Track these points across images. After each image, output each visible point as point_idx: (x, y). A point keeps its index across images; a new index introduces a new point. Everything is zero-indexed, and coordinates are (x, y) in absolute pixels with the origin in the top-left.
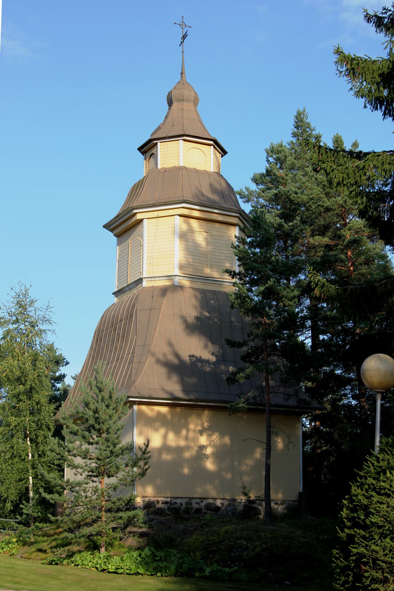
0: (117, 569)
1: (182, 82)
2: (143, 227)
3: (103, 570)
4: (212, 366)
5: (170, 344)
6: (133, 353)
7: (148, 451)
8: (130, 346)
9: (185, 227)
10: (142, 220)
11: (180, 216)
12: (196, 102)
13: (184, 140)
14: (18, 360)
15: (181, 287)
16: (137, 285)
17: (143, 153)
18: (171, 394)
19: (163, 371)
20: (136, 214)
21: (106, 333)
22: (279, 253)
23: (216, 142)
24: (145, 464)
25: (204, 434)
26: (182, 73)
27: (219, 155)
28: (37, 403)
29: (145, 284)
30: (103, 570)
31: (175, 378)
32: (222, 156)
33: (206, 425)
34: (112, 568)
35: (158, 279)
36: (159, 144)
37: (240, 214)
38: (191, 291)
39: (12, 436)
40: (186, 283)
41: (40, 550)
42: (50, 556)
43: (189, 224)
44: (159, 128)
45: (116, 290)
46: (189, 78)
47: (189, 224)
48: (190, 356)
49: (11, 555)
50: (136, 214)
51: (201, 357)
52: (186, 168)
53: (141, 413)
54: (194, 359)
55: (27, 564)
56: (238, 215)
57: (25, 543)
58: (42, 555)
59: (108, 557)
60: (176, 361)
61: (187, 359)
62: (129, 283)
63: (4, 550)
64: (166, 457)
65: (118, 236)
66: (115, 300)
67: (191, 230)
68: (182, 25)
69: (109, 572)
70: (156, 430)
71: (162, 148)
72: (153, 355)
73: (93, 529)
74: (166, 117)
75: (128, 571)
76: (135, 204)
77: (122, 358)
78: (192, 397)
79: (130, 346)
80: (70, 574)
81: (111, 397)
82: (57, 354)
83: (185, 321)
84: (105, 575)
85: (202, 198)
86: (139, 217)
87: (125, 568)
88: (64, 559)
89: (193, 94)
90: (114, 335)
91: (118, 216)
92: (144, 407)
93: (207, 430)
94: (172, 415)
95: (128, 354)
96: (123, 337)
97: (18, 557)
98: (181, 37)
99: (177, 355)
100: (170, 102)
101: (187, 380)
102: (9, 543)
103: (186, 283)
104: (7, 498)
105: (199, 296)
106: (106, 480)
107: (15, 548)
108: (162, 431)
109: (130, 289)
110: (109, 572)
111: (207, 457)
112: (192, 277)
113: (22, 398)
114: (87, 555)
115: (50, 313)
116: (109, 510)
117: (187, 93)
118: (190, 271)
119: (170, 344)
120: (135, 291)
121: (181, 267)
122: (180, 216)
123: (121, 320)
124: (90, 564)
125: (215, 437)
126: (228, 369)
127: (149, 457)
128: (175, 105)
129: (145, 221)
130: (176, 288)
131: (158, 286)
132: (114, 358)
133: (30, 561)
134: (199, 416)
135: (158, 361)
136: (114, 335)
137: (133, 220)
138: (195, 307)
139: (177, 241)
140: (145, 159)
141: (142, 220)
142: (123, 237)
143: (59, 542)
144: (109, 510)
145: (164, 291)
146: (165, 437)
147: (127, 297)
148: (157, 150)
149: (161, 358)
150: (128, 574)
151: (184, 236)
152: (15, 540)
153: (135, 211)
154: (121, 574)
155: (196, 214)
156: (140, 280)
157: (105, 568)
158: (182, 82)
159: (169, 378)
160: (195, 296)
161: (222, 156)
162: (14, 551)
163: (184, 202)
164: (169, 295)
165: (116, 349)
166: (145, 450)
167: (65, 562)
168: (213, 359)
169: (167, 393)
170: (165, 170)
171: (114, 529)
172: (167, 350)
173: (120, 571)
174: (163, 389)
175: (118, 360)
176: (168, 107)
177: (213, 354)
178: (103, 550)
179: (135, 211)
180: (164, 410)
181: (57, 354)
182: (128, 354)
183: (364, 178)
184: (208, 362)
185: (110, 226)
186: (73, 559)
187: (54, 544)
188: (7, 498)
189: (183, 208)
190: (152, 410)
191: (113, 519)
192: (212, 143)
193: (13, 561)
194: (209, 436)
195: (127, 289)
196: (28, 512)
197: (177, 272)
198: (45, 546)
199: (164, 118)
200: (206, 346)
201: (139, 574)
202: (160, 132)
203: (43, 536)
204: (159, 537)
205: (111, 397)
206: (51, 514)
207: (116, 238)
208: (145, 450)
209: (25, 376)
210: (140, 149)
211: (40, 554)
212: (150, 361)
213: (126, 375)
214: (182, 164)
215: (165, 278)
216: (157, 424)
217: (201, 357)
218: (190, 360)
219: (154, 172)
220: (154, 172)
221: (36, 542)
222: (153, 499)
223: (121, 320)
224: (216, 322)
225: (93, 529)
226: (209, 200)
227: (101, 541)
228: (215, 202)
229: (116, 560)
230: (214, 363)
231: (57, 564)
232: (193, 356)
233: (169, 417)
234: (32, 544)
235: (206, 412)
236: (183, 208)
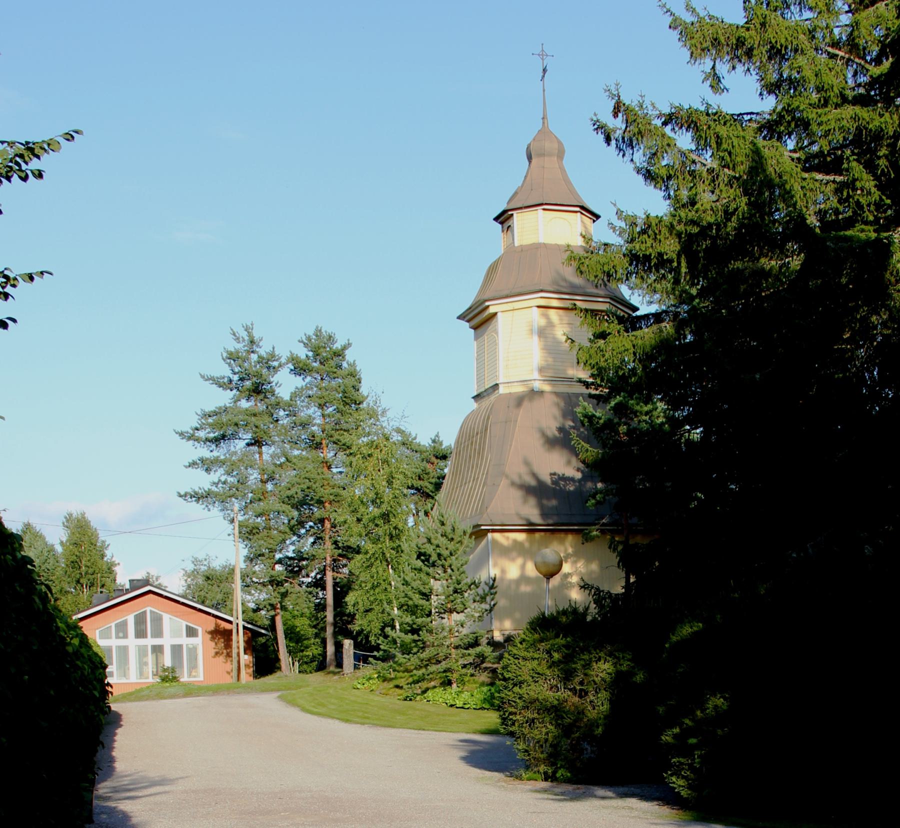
0: (465, 704)
1: (544, 132)
2: (497, 321)
3: (452, 706)
4: (577, 484)
5: (527, 463)
6: (487, 473)
7: (495, 585)
8: (485, 468)
9: (543, 322)
10: (495, 314)
11: (539, 307)
12: (561, 154)
13: (544, 209)
14: (372, 479)
15: (541, 393)
16: (494, 391)
17: (502, 223)
18: (528, 520)
19: (518, 494)
20: (488, 306)
21: (464, 447)
22: (347, 551)
23: (583, 208)
24: (492, 599)
25: (569, 560)
26: (543, 118)
27: (588, 221)
28: (395, 528)
29: (502, 390)
30: (452, 706)
31: (532, 501)
32: (594, 221)
33: (570, 550)
34: (459, 703)
35: (516, 384)
36: (515, 215)
37: (611, 298)
38: (554, 399)
39: (372, 565)
40: (547, 388)
41: (397, 687)
42: (404, 693)
43: (546, 316)
44: (516, 193)
45: (475, 394)
46: (553, 127)
47: (546, 316)
48: (551, 474)
49: (372, 691)
50: (488, 306)
51: (564, 475)
52: (545, 245)
53: (495, 542)
54: (556, 477)
55: (383, 700)
56: (608, 300)
57: (385, 680)
58: (398, 691)
59: (459, 693)
60: (533, 483)
61: (547, 479)
62: (486, 388)
63: (365, 686)
64: (525, 589)
65: (475, 328)
66: (474, 405)
67: (550, 324)
68: (543, 55)
69: (457, 708)
70: (513, 560)
71: (518, 219)
72: (507, 477)
73: (444, 665)
74: (526, 177)
75: (474, 706)
76: (486, 297)
77: (478, 478)
78: (551, 522)
79: (485, 468)
80: (418, 710)
81: (454, 530)
82: (443, 447)
83: (543, 434)
84: (453, 709)
85: (563, 284)
86: (492, 310)
87: (472, 703)
88: (418, 695)
89: (556, 145)
90: (471, 450)
91: (470, 308)
92: (497, 536)
93: (572, 555)
94: (531, 542)
95: (483, 474)
96: (479, 453)
97: (378, 693)
98: (542, 70)
99: (534, 475)
100: (530, 158)
101: (545, 502)
102: (370, 679)
103: (547, 388)
104: (370, 632)
105: (562, 404)
106: (455, 616)
107: (375, 683)
108: (520, 561)
109: (488, 395)
110: (457, 708)
111: (572, 586)
112: (552, 381)
113: (379, 523)
114: (440, 690)
115: (406, 424)
116: (456, 647)
117: (548, 145)
118: (550, 373)
119: (527, 463)
120: (493, 398)
121: (541, 370)
122: (539, 307)
123: (477, 434)
124: (441, 700)
125: (580, 565)
126: (596, 486)
127: (496, 593)
128: (534, 161)
129: (499, 314)
130: (534, 394)
131: (515, 393)
132: (471, 477)
133: (388, 697)
134: (562, 542)
135: (513, 484)
136: (471, 450)
137: (486, 313)
138: (555, 418)
139: (536, 338)
140: (503, 231)
141: (495, 314)
142: (479, 331)
143: (416, 678)
144: (456, 647)
145: (519, 400)
146: (523, 567)
147: (486, 402)
148: (513, 223)
149: (517, 480)
150: (474, 709)
151: (542, 333)
152: (376, 676)
153: (487, 304)
154: (468, 708)
155: (555, 303)
156: (496, 386)
157: (454, 703)
158: (544, 132)
159: (525, 501)
160: (558, 405)
161: (594, 221)
162: (374, 687)
163: (542, 291)
164: (526, 404)
165: (473, 467)
166: (493, 584)
167: (418, 698)
168: (579, 476)
169: (522, 518)
170: (523, 248)
171: (464, 666)
172: (523, 470)
173: (466, 706)
174: (518, 515)
175: (474, 480)
176: (528, 163)
177: (578, 470)
178: (454, 686)
179: (487, 304)
180: (521, 537)
181: (443, 447)
182: (483, 474)
183: (602, 360)
184: (572, 479)
185: (464, 317)
186: (425, 695)
187: (411, 680)
188: (370, 632)
189: (541, 297)
190: (508, 538)
191: (461, 655)
192: (578, 209)
193: (371, 697)
194: (575, 562)
195: (485, 394)
196: (386, 648)
197: (536, 375)
198: (402, 682)
199: (523, 179)
200: (569, 463)
201: (485, 709)
202: (516, 199)
203: (404, 672)
204: (439, 662)
205: (454, 530)
206: (357, 646)
207: (473, 331)
208: (493, 584)
209: (380, 498)
210: (496, 219)
211: (397, 690)
212: (504, 483)
213: (479, 500)
214: (542, 241)
215: (519, 384)
216: (514, 554)
217: (564, 475)
218: (551, 478)
219: (511, 249)
220: (511, 249)
221: (395, 678)
222: (513, 633)
223: (477, 434)
224: (582, 432)
225: (444, 665)
226: (573, 286)
227: (454, 677)
228: (580, 287)
229: (466, 695)
230: (580, 481)
231: (411, 700)
232: (554, 474)
233: (527, 545)
234: (391, 679)
235: (570, 537)
236: (541, 297)
